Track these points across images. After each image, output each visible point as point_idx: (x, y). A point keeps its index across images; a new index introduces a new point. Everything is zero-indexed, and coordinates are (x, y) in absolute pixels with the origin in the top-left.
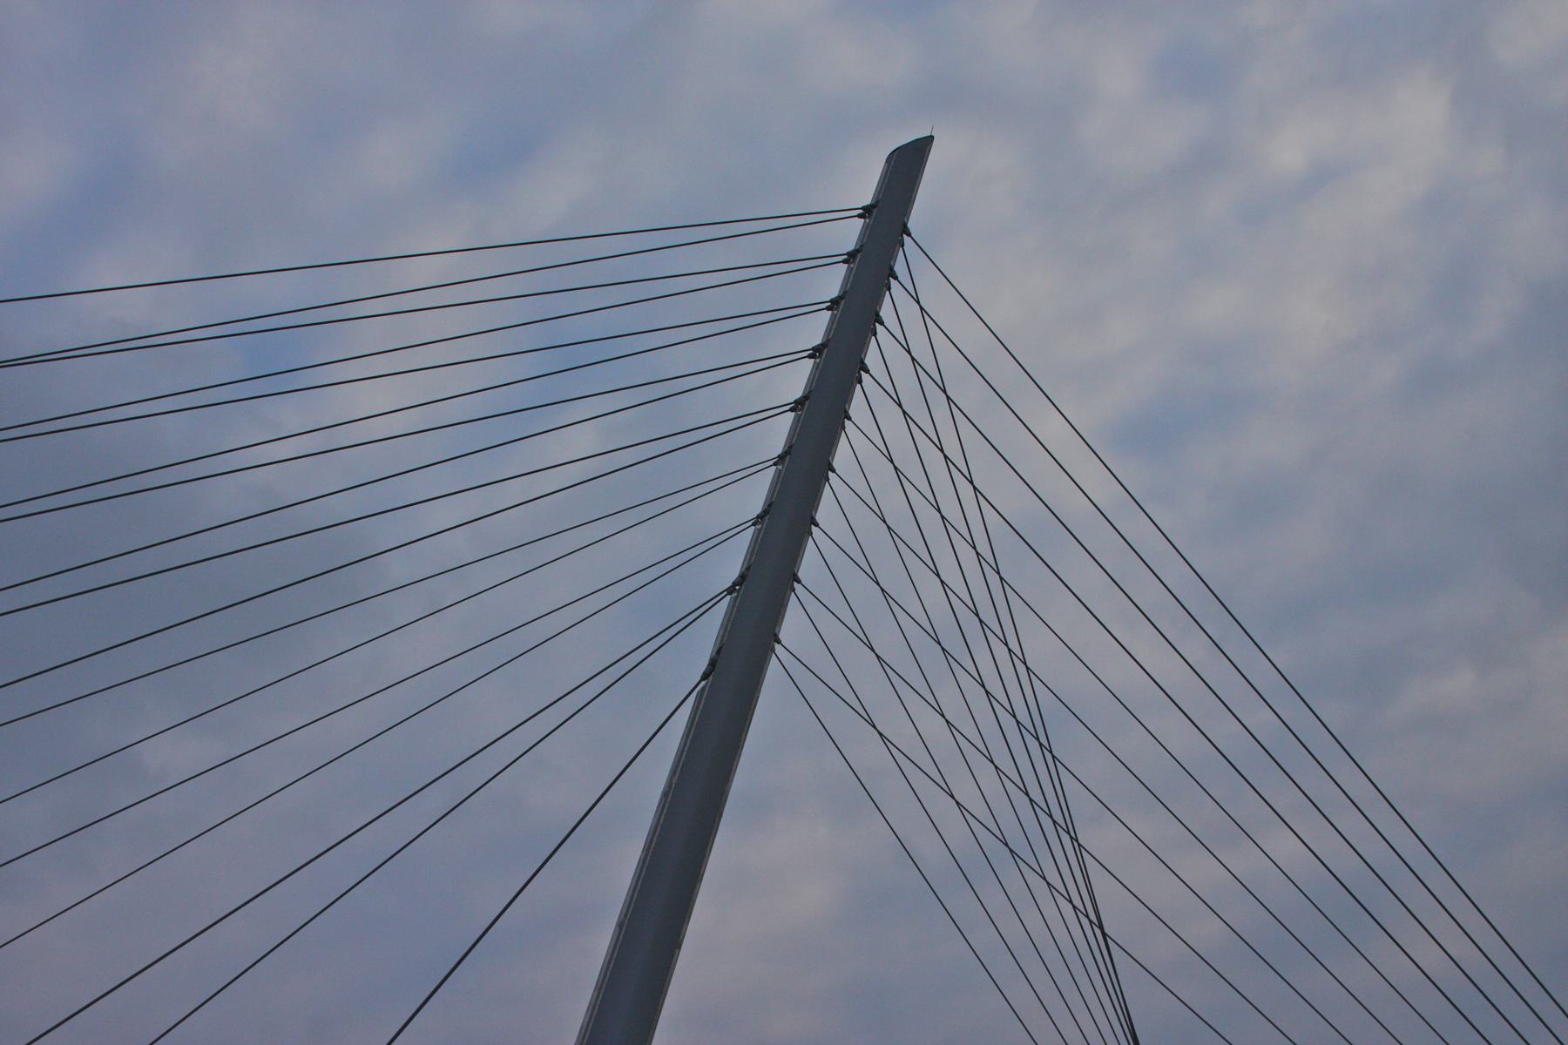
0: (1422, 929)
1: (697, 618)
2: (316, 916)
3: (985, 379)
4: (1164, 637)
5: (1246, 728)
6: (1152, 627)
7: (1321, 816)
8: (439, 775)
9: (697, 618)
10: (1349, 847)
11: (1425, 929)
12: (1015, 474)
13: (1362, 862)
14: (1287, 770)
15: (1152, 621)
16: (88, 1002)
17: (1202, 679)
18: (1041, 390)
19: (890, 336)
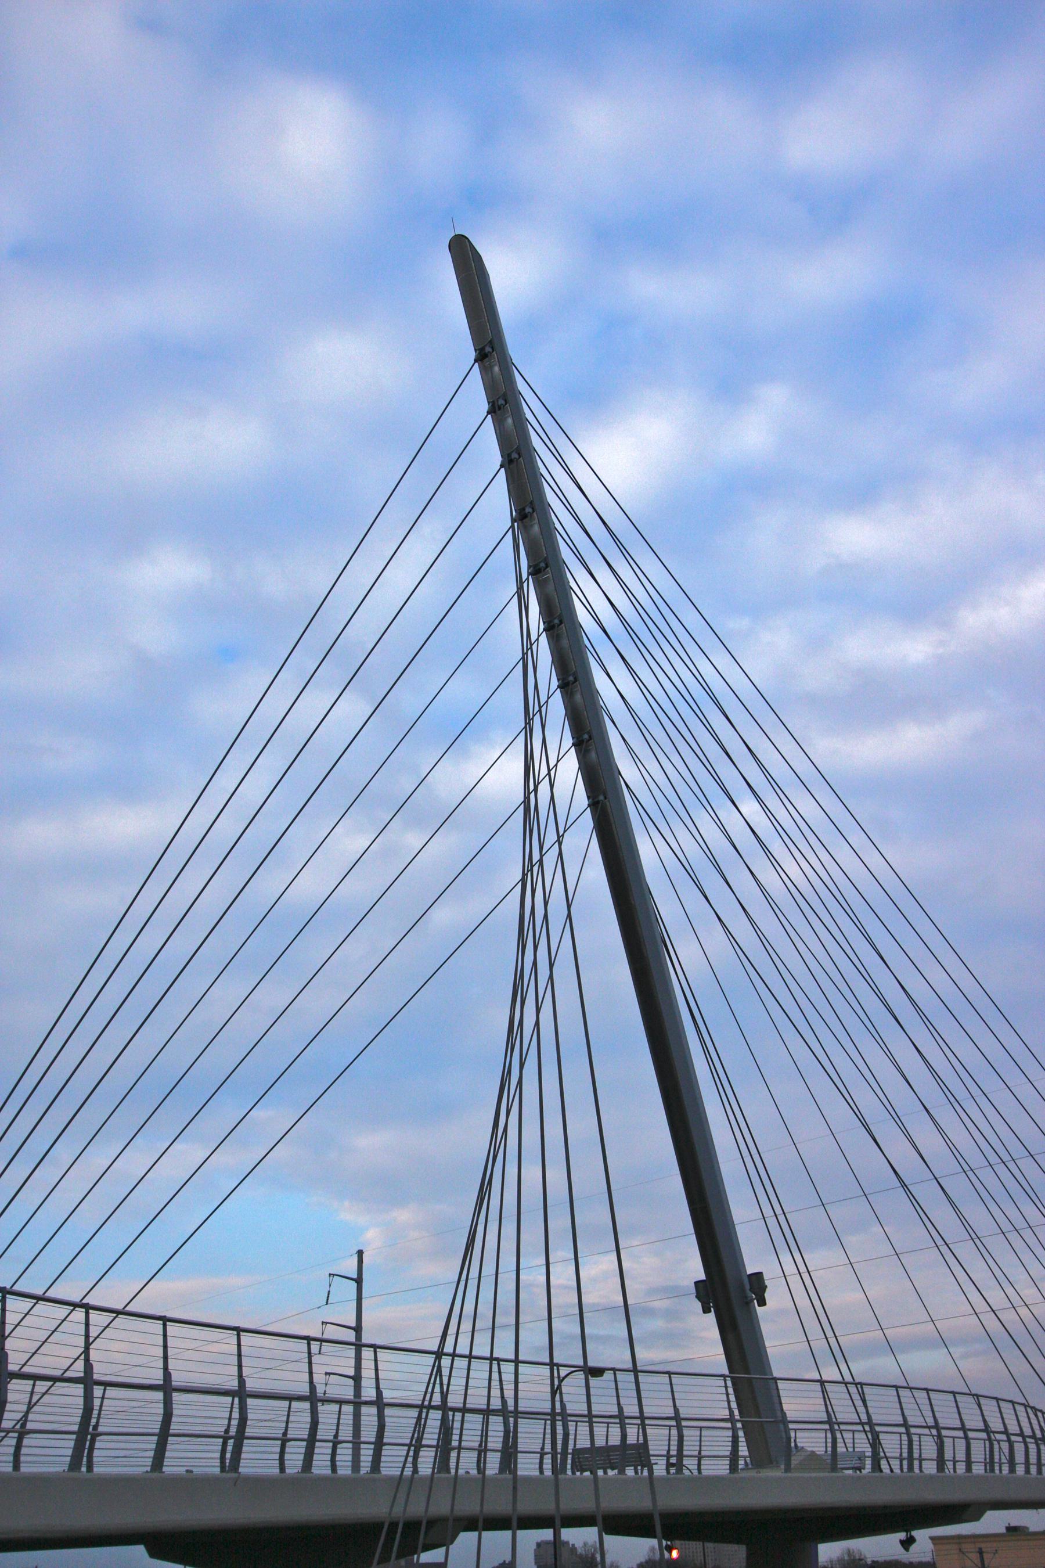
0: (436, 426)
1: (867, 981)
2: (834, 963)
3: (806, 964)
4: (660, 612)
5: (782, 880)
6: (783, 826)
7: (741, 699)
8: (319, 606)
9: (867, 981)
10: (800, 1313)
11: (675, 635)
12: (179, 1194)
13: (599, 654)
14: (654, 677)
15: (770, 1198)
16: (667, 845)
17: (895, 872)
18: (645, 825)
19: (721, 678)
